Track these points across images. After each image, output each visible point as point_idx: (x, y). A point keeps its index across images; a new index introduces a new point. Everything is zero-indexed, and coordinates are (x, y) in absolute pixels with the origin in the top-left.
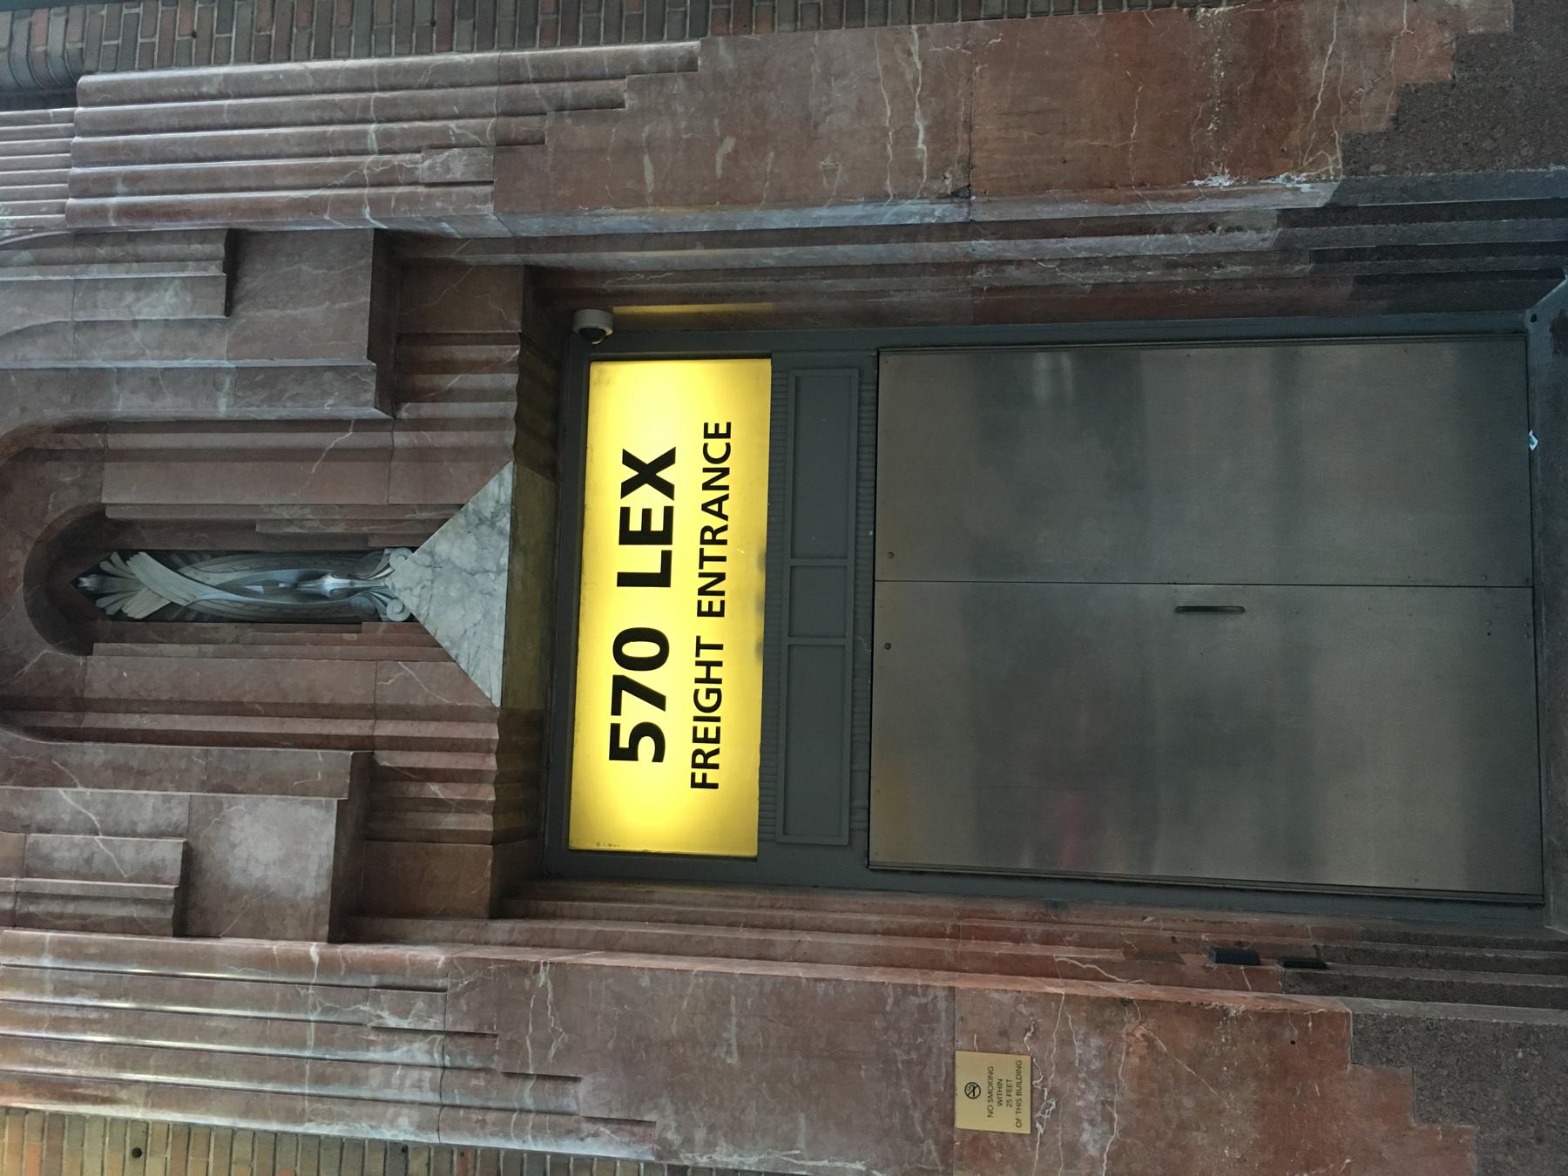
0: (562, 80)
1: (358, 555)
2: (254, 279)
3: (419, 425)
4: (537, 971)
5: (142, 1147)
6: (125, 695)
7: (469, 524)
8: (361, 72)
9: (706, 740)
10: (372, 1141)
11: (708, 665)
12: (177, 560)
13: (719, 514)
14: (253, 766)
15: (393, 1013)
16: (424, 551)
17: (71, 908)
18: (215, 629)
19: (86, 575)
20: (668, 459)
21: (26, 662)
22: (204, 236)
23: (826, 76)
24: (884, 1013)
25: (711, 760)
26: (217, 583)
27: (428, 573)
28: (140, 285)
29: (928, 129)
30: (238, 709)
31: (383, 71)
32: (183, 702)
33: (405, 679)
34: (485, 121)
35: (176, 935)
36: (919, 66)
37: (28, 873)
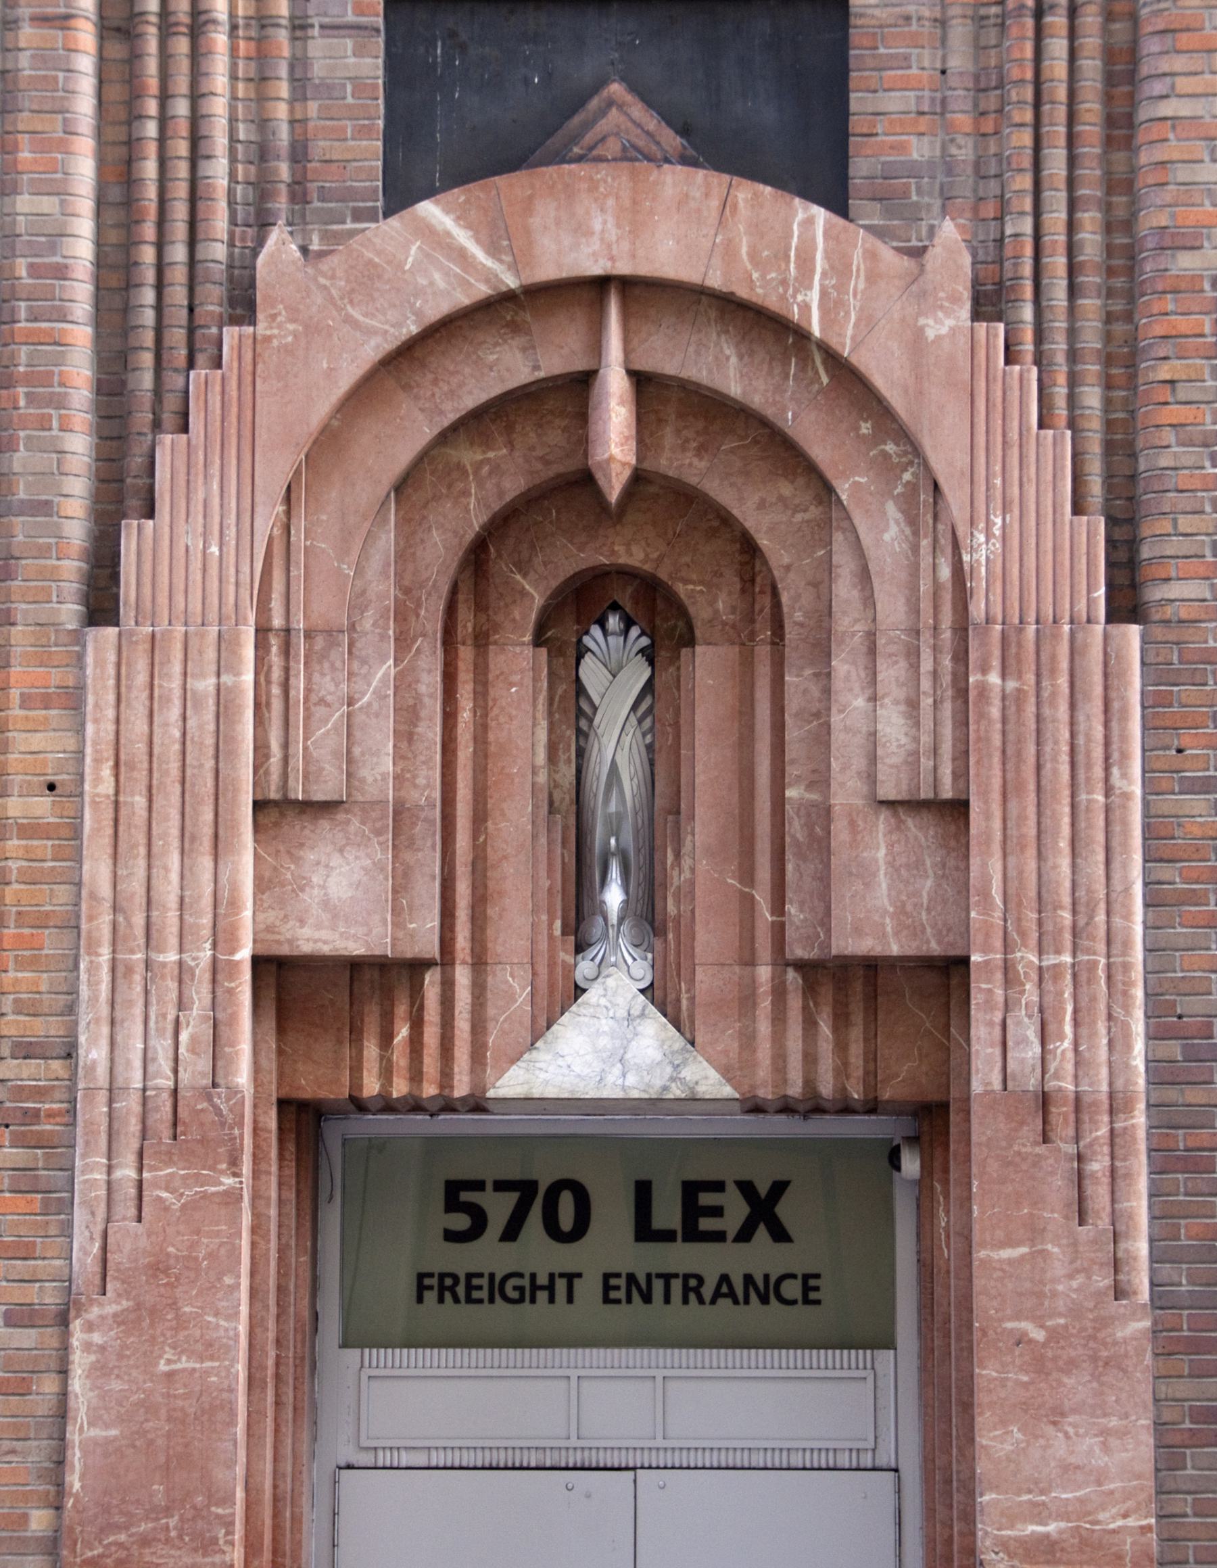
0: (1113, 1157)
2: (921, 832)
3: (779, 992)
4: (235, 1175)
5: (57, 792)
6: (492, 693)
8: (1127, 945)
9: (469, 1288)
10: (76, 1023)
11: (551, 1288)
13: (717, 1295)
14: (420, 854)
20: (780, 1234)
21: (525, 576)
22: (961, 774)
23: (1105, 1432)
24: (208, 1506)
25: (447, 1295)
26: (618, 759)
27: (622, 1013)
28: (913, 704)
29: (1047, 1536)
30: (480, 818)
32: (486, 756)
33: (514, 986)
34: (1070, 1078)
35: (255, 803)
36: (1112, 1526)
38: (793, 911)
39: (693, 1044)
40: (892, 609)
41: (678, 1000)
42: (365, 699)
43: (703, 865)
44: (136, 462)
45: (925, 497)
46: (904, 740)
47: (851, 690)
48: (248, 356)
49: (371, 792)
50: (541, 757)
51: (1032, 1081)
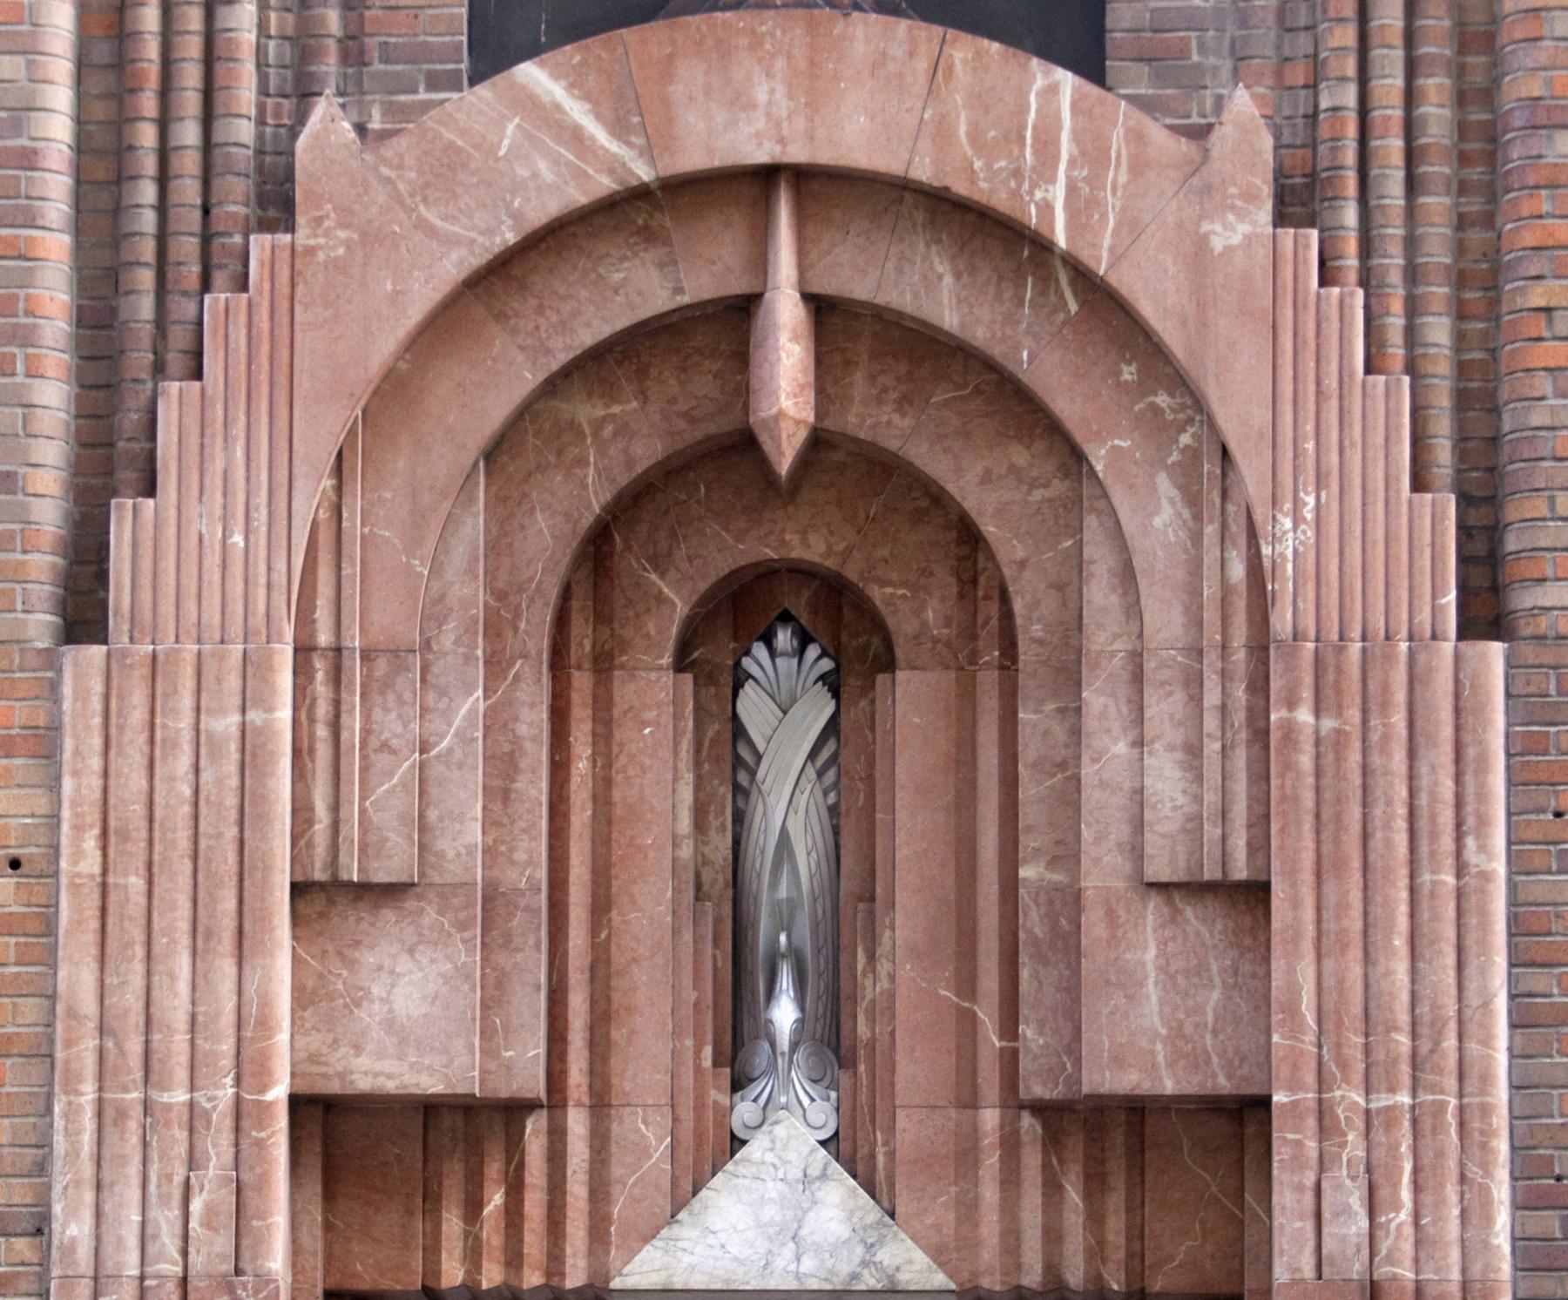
1: (833, 1043)
2: (1203, 926)
3: (1010, 1145)
6: (618, 734)
8: (1486, 1079)
10: (49, 1187)
14: (519, 957)
18: (723, 827)
21: (662, 576)
22: (1260, 846)
28: (1193, 751)
30: (601, 907)
31: (1486, 1111)
32: (609, 823)
33: (647, 1137)
34: (1408, 1263)
38: (1029, 1033)
39: (892, 1215)
40: (1164, 620)
41: (873, 1156)
42: (445, 744)
43: (906, 971)
44: (131, 419)
45: (1211, 467)
46: (1181, 800)
47: (1108, 731)
48: (284, 275)
51: (1357, 1266)
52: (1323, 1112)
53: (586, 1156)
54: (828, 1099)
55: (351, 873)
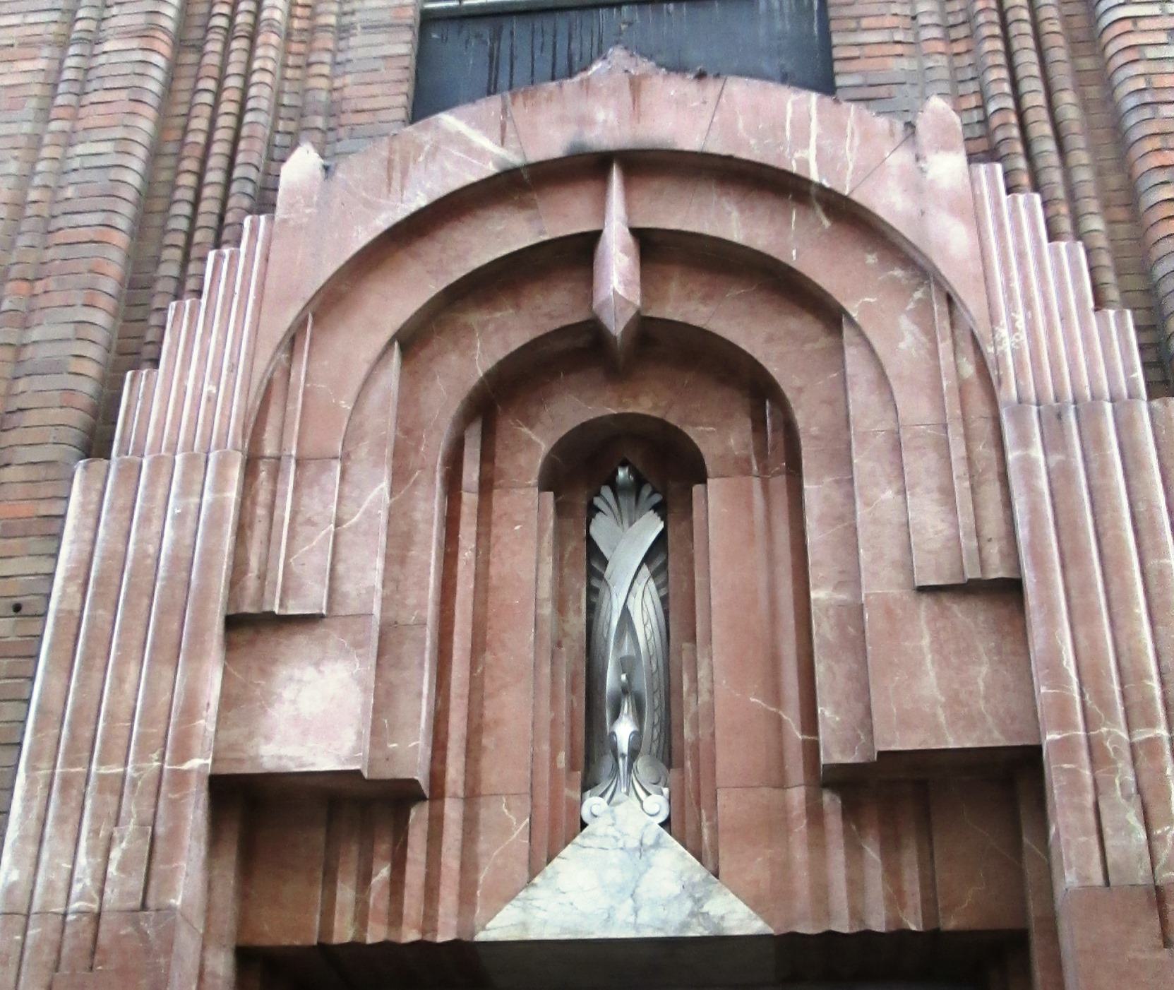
1: (667, 751)
2: (968, 617)
3: (815, 815)
5: (23, 611)
6: (495, 531)
7: (694, 885)
12: (658, 562)
15: (125, 852)
16: (659, 836)
17: (261, 511)
18: (579, 609)
19: (633, 471)
28: (947, 493)
30: (478, 646)
32: (486, 591)
33: (508, 826)
37: (298, 463)
38: (827, 713)
39: (717, 876)
40: (916, 409)
41: (699, 830)
42: (355, 519)
43: (722, 683)
45: (939, 308)
46: (941, 526)
47: (877, 485)
49: (352, 606)
50: (547, 610)
51: (1142, 873)
52: (1093, 747)
53: (459, 837)
54: (662, 793)
55: (273, 604)
